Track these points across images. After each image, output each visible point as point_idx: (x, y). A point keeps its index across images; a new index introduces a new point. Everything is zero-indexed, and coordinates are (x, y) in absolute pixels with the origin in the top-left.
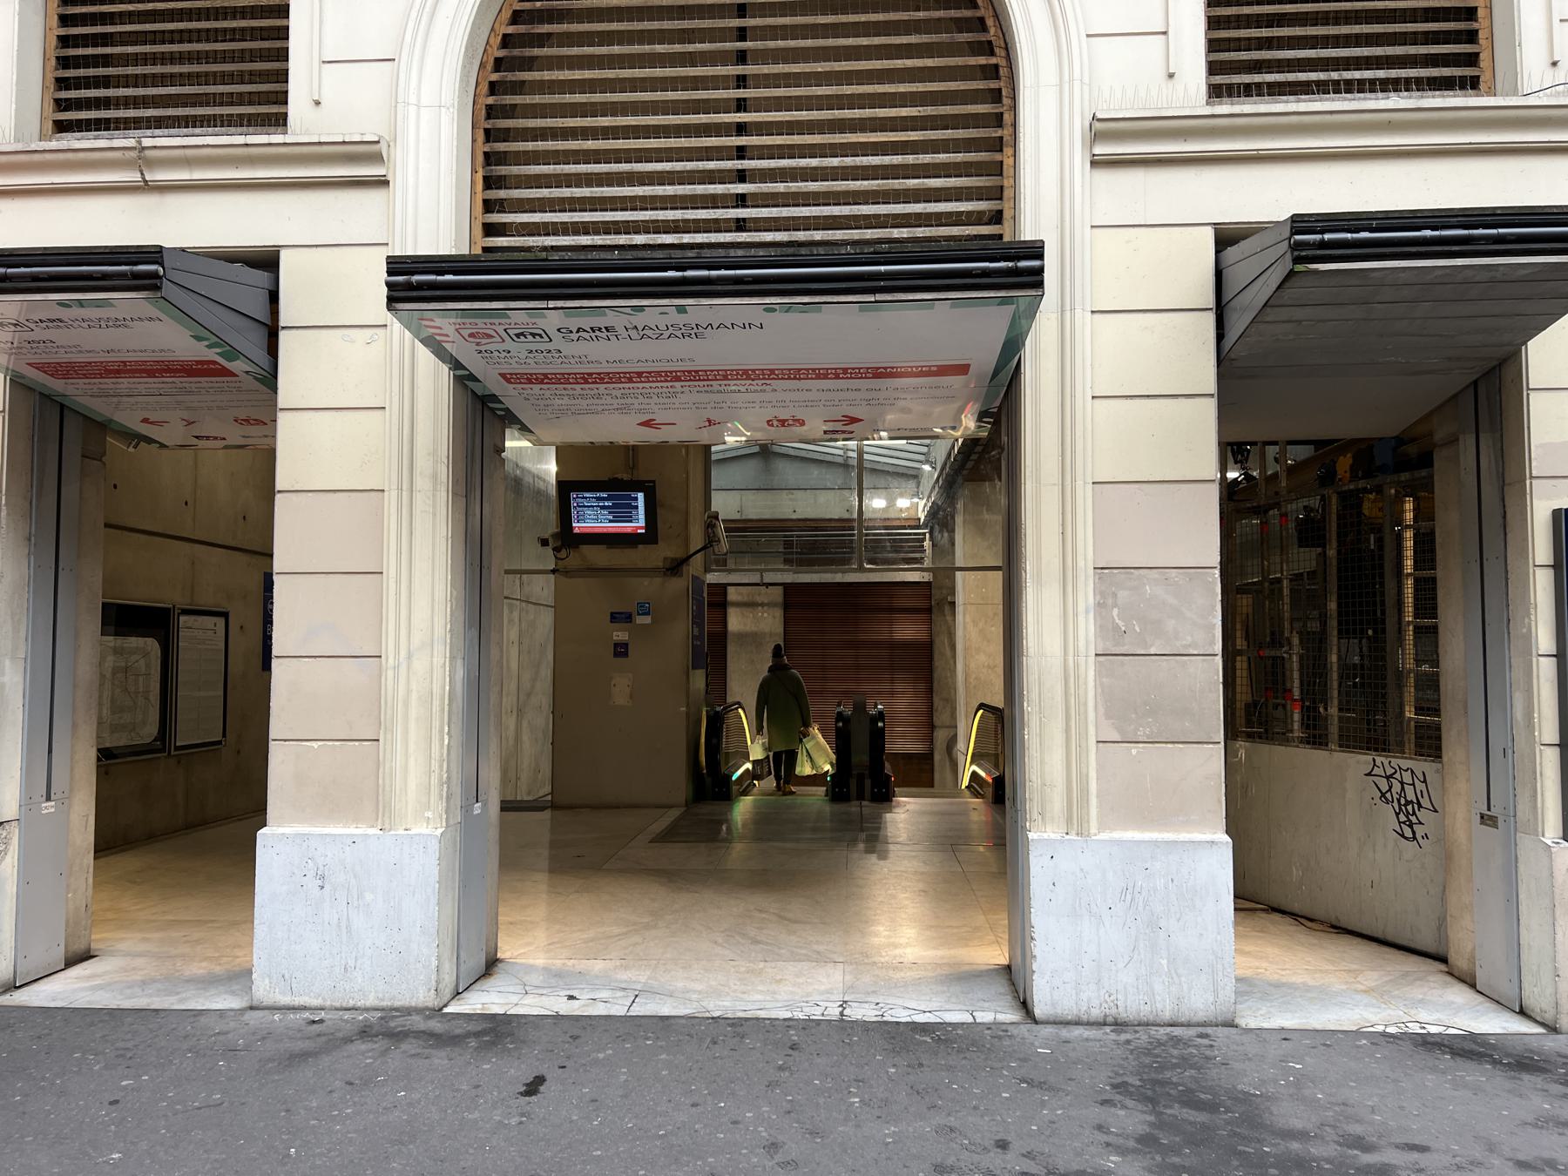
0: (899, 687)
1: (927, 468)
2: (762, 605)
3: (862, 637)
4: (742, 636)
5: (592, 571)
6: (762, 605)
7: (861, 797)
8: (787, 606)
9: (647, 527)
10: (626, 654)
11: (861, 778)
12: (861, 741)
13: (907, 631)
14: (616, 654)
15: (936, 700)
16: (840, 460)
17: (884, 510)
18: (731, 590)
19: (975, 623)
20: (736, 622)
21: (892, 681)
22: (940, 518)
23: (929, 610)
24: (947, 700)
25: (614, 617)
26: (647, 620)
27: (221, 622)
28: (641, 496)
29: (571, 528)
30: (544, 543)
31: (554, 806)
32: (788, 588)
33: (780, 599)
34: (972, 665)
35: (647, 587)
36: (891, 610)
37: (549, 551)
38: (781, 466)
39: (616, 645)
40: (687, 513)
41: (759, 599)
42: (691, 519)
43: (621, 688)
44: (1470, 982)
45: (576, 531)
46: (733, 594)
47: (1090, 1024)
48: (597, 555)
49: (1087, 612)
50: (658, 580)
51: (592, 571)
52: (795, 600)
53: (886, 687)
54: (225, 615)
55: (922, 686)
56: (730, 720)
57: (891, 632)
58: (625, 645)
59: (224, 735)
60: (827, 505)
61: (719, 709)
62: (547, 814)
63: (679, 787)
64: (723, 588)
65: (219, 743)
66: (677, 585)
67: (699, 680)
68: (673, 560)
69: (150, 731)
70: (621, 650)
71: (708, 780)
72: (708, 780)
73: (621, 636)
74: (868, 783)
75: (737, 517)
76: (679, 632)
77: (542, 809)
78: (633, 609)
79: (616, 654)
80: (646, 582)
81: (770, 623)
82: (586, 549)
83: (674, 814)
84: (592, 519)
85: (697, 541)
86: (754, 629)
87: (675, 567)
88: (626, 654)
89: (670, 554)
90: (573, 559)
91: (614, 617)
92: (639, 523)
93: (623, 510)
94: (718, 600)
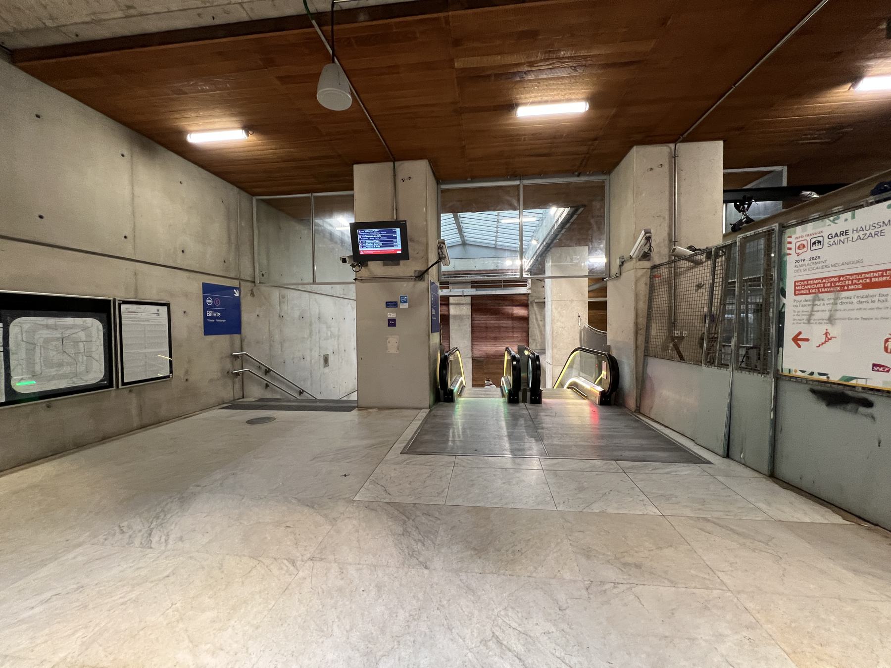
3: (501, 315)
4: (455, 316)
5: (375, 279)
7: (524, 401)
8: (472, 305)
10: (394, 325)
13: (518, 313)
14: (389, 325)
18: (451, 298)
19: (556, 309)
20: (453, 311)
22: (538, 269)
23: (527, 305)
25: (388, 304)
26: (406, 306)
27: (164, 309)
28: (398, 230)
31: (360, 408)
32: (473, 297)
34: (555, 327)
35: (406, 288)
37: (348, 266)
39: (389, 320)
42: (429, 250)
43: (393, 342)
44: (132, 175)
45: (362, 253)
46: (452, 300)
47: (293, 160)
48: (376, 268)
50: (411, 283)
51: (375, 279)
52: (476, 302)
53: (511, 335)
54: (168, 305)
55: (525, 334)
56: (452, 358)
58: (394, 320)
59: (171, 372)
62: (354, 414)
63: (425, 396)
64: (448, 297)
65: (168, 377)
66: (422, 285)
67: (436, 338)
68: (419, 271)
69: (97, 373)
70: (392, 323)
71: (442, 392)
72: (442, 392)
73: (392, 314)
74: (529, 394)
76: (424, 312)
77: (349, 409)
78: (397, 299)
79: (389, 325)
80: (405, 284)
81: (466, 310)
82: (372, 265)
83: (423, 414)
84: (371, 245)
85: (433, 258)
87: (421, 276)
88: (394, 325)
90: (364, 272)
91: (388, 304)
92: (397, 248)
93: (388, 241)
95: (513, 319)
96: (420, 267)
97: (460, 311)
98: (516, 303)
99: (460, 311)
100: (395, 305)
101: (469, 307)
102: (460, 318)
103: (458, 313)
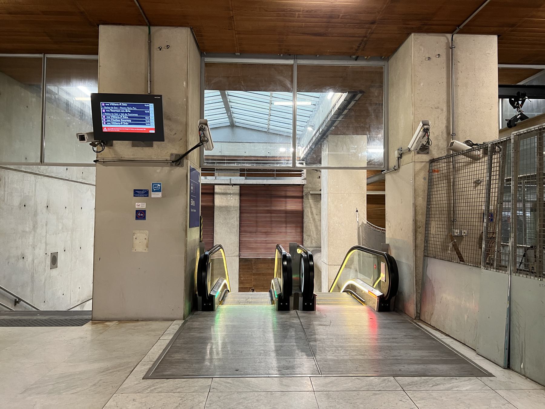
0: (289, 230)
1: (310, 129)
2: (230, 194)
3: (274, 208)
4: (221, 208)
5: (121, 161)
6: (230, 194)
7: (296, 308)
8: (241, 195)
9: (156, 129)
10: (144, 218)
11: (296, 296)
12: (299, 277)
13: (292, 206)
14: (137, 218)
15: (304, 235)
16: (266, 130)
17: (285, 153)
20: (218, 201)
21: (286, 227)
22: (314, 157)
23: (302, 197)
24: (309, 236)
25: (136, 193)
26: (159, 195)
28: (151, 106)
29: (102, 128)
30: (82, 138)
32: (242, 187)
33: (238, 192)
35: (159, 174)
36: (286, 197)
37: (86, 144)
38: (238, 131)
39: (137, 212)
40: (187, 124)
41: (228, 191)
43: (141, 239)
45: (105, 130)
46: (217, 189)
48: (123, 149)
49: (257, 206)
50: (166, 169)
51: (121, 161)
52: (245, 192)
53: (283, 230)
55: (299, 230)
57: (286, 206)
58: (144, 212)
60: (259, 150)
61: (207, 253)
63: (177, 300)
66: (179, 172)
67: (195, 234)
68: (176, 155)
70: (141, 215)
73: (140, 205)
74: (301, 299)
75: (220, 154)
76: (181, 204)
77: (80, 322)
78: (149, 187)
79: (137, 218)
80: (159, 169)
81: (234, 201)
83: (175, 326)
84: (114, 123)
85: (193, 140)
86: (227, 205)
87: (178, 160)
88: (144, 218)
89: (175, 152)
91: (136, 193)
92: (150, 126)
94: (209, 191)
95: (286, 212)
96: (177, 150)
97: (227, 202)
98: (289, 194)
99: (227, 202)
100: (146, 193)
101: (237, 198)
102: (226, 209)
103: (224, 204)
